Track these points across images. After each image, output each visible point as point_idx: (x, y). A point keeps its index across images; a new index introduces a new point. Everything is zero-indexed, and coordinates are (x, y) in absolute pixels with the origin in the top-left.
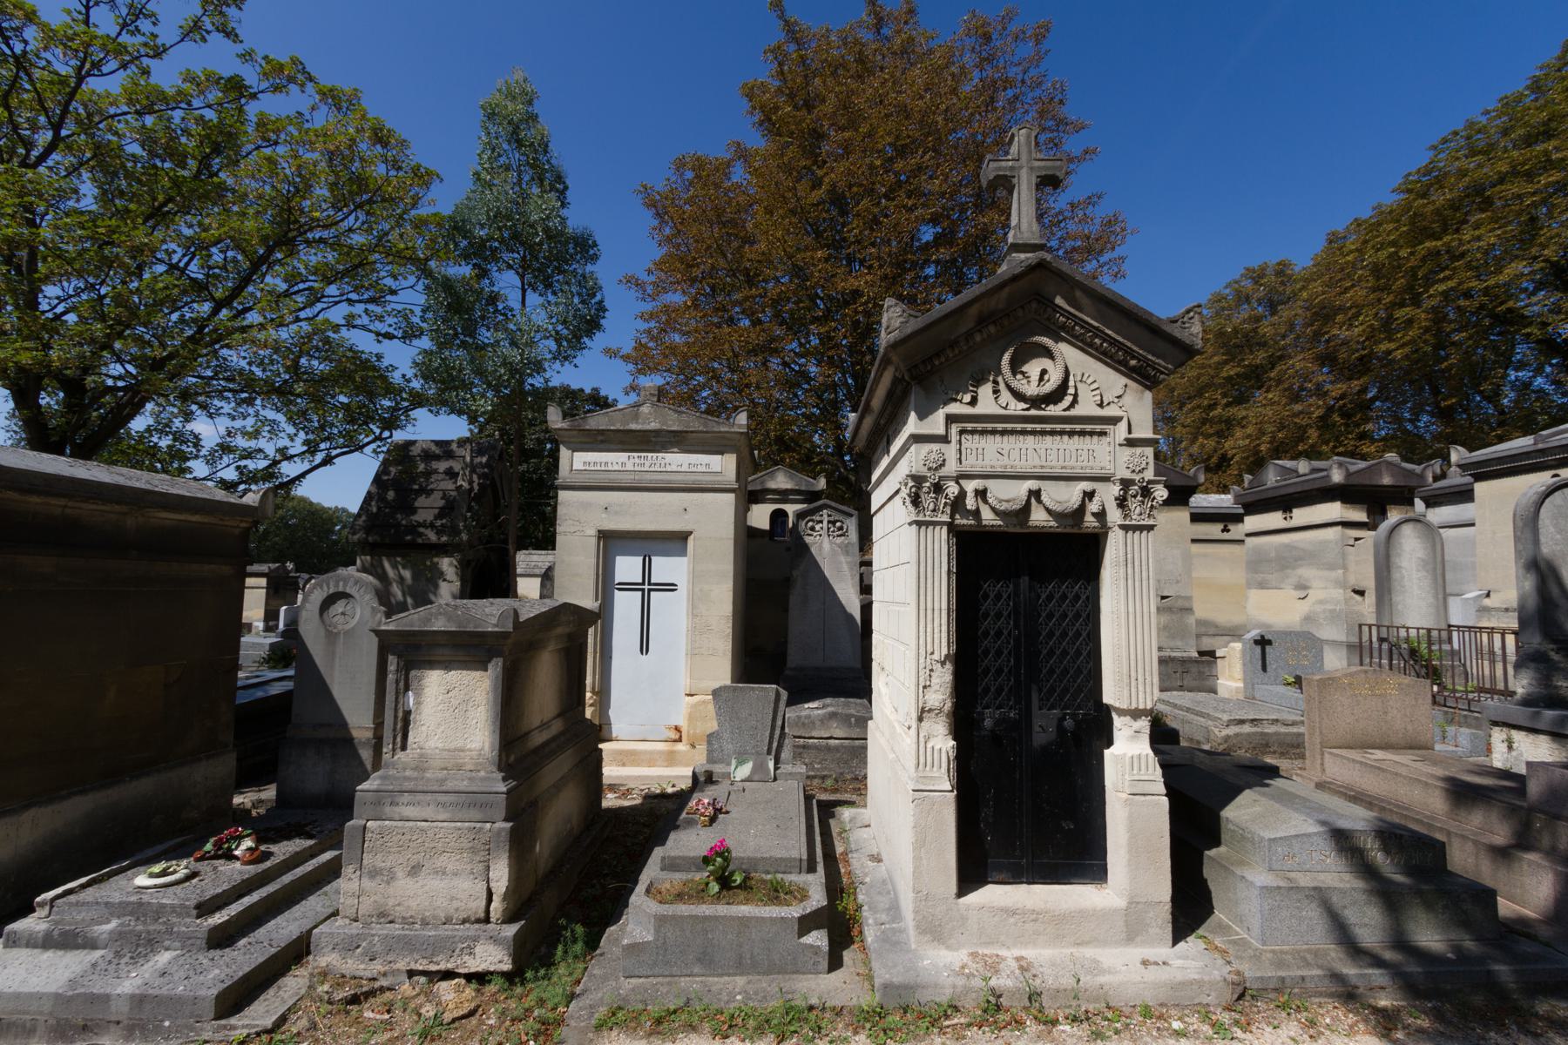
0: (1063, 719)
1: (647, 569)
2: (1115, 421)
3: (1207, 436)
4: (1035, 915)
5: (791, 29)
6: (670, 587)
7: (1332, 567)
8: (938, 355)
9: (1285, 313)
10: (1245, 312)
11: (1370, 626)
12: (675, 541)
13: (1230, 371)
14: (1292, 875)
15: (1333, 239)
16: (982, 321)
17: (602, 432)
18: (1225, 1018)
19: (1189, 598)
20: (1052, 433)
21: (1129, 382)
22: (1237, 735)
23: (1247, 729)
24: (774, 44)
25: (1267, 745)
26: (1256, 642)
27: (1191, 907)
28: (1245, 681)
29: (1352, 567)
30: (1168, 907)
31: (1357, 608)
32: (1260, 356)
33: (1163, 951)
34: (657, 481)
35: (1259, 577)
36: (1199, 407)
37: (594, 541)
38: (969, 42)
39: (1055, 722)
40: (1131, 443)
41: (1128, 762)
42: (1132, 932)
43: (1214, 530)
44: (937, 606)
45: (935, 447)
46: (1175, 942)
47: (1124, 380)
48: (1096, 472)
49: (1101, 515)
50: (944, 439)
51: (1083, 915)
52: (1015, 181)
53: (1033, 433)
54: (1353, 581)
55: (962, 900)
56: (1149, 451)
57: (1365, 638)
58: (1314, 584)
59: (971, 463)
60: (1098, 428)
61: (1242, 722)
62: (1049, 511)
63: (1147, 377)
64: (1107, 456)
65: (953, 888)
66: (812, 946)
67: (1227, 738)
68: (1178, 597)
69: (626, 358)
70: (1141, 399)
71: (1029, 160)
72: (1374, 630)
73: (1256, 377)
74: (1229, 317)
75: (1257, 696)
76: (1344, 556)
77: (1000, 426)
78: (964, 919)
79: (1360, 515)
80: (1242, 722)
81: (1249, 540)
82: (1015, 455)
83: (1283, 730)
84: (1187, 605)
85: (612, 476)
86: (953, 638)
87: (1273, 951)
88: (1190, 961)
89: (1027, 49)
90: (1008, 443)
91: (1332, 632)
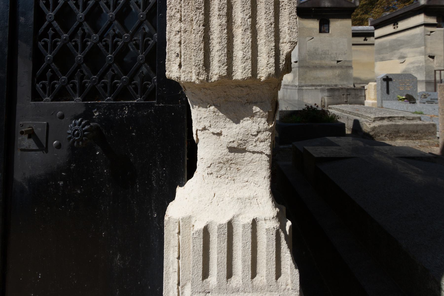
7: (418, 46)
19: (350, 61)
22: (380, 126)
23: (385, 123)
26: (384, 80)
28: (378, 100)
29: (429, 45)
35: (381, 56)
43: (361, 40)
54: (429, 52)
61: (382, 119)
67: (374, 129)
68: (345, 61)
76: (425, 40)
80: (382, 119)
81: (377, 42)
83: (408, 122)
84: (349, 65)
91: (421, 77)
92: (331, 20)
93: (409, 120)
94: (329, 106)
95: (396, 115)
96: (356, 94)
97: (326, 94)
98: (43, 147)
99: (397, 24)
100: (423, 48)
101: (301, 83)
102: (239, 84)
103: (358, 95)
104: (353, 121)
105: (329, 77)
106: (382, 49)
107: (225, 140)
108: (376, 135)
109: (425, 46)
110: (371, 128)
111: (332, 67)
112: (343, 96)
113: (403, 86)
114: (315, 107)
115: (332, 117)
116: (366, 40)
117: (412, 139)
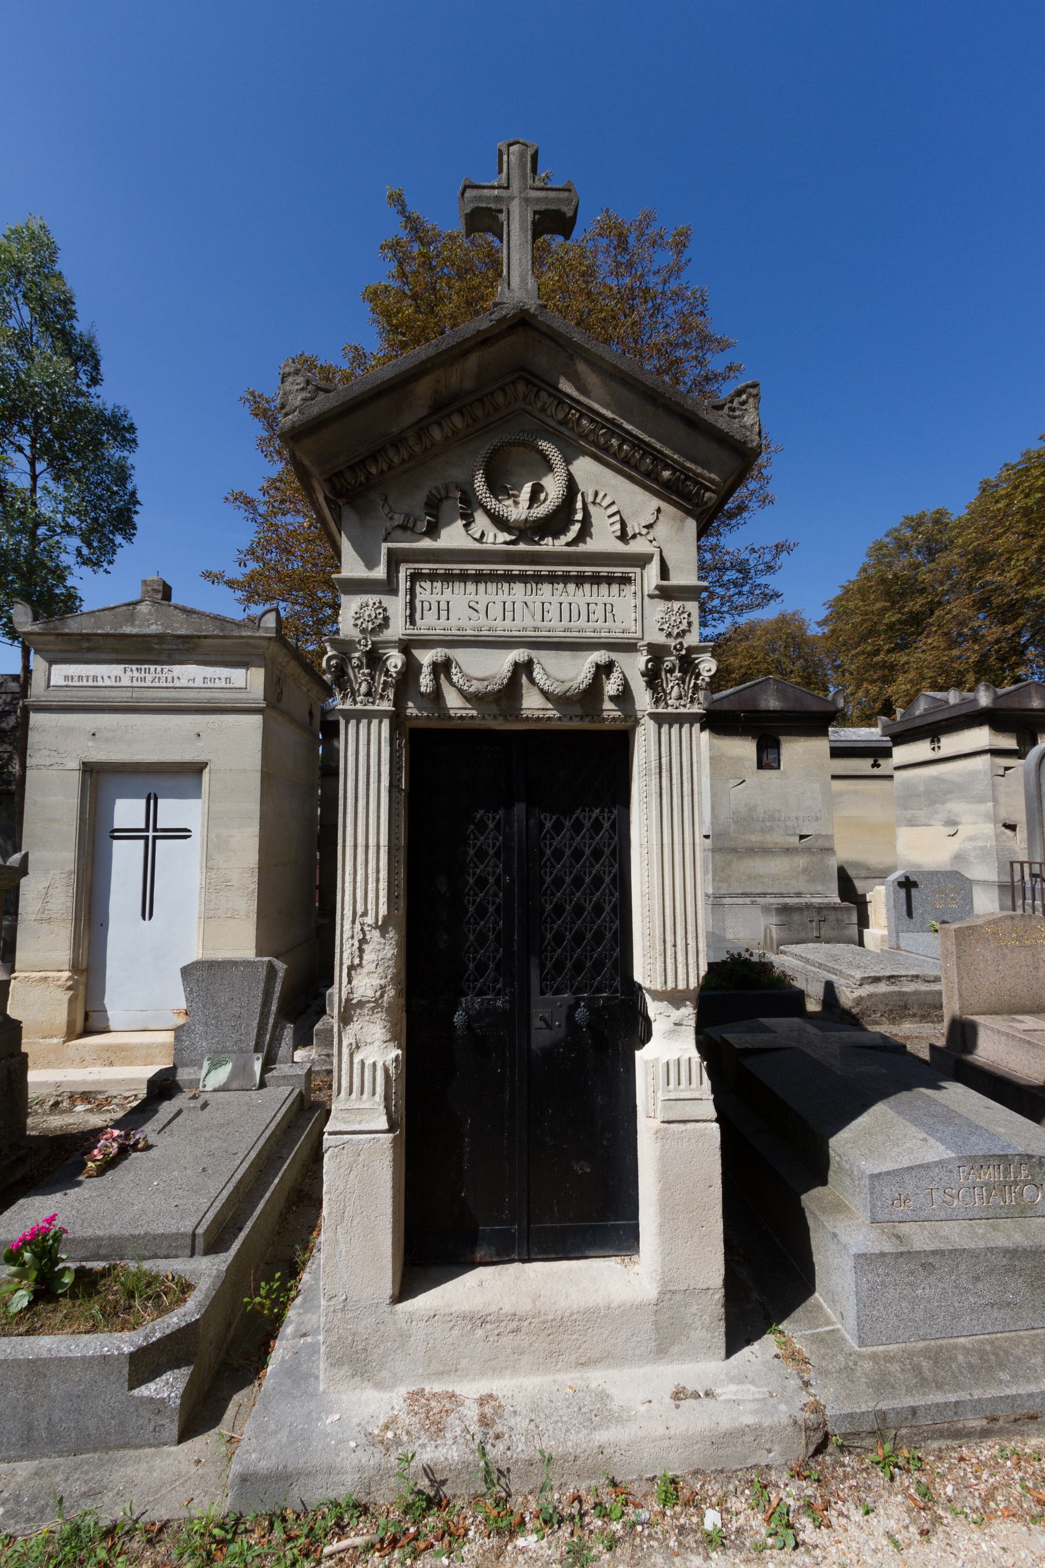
0: (576, 1006)
1: (151, 814)
2: (642, 561)
3: (873, 682)
4: (515, 1323)
5: (414, 226)
6: (181, 834)
7: (981, 800)
8: (373, 457)
9: (944, 559)
10: (904, 560)
11: (1022, 864)
12: (186, 776)
13: (891, 617)
14: (905, 1229)
15: (986, 487)
16: (442, 407)
17: (87, 637)
18: (790, 1493)
19: (830, 837)
20: (552, 579)
21: (664, 506)
23: (883, 988)
24: (390, 239)
25: (906, 1007)
26: (901, 884)
27: (765, 1275)
28: (888, 927)
29: (1002, 799)
30: (719, 1295)
31: (1008, 844)
32: (917, 604)
33: (707, 1366)
34: (161, 700)
35: (908, 814)
36: (863, 653)
37: (77, 776)
38: (603, 243)
39: (564, 1011)
40: (666, 593)
41: (668, 1068)
42: (665, 1337)
43: (863, 765)
44: (372, 842)
45: (372, 599)
46: (732, 1348)
47: (656, 503)
48: (617, 635)
49: (624, 697)
50: (389, 587)
51: (592, 1317)
52: (503, 217)
53: (523, 578)
54: (1004, 815)
55: (401, 1307)
56: (693, 607)
57: (1017, 877)
58: (964, 819)
59: (428, 624)
60: (618, 571)
61: (877, 980)
62: (545, 694)
63: (687, 497)
64: (633, 613)
65: (386, 1285)
66: (151, 1400)
67: (859, 1000)
68: (819, 836)
69: (231, 584)
70: (681, 529)
71: (523, 189)
72: (1026, 867)
73: (916, 621)
74: (890, 565)
75: (902, 945)
77: (472, 568)
78: (404, 1337)
79: (1009, 743)
80: (877, 980)
81: (899, 775)
82: (496, 611)
84: (827, 845)
85: (102, 694)
86: (401, 891)
87: (874, 1357)
88: (750, 1390)
89: (665, 257)
90: (487, 595)
91: (984, 870)
92: (782, 738)
93: (929, 981)
94: (782, 948)
95: (903, 973)
96: (837, 920)
97: (774, 919)
98: (549, 1027)
99: (939, 741)
100: (990, 804)
101: (719, 888)
102: (680, 991)
103: (842, 921)
104: (823, 985)
105: (782, 874)
106: (908, 798)
107: (672, 1019)
108: (863, 1014)
109: (995, 800)
110: (854, 1000)
111: (788, 851)
112: (810, 925)
113: (942, 898)
114: (747, 955)
115: (779, 977)
116: (878, 766)
117: (933, 1022)
